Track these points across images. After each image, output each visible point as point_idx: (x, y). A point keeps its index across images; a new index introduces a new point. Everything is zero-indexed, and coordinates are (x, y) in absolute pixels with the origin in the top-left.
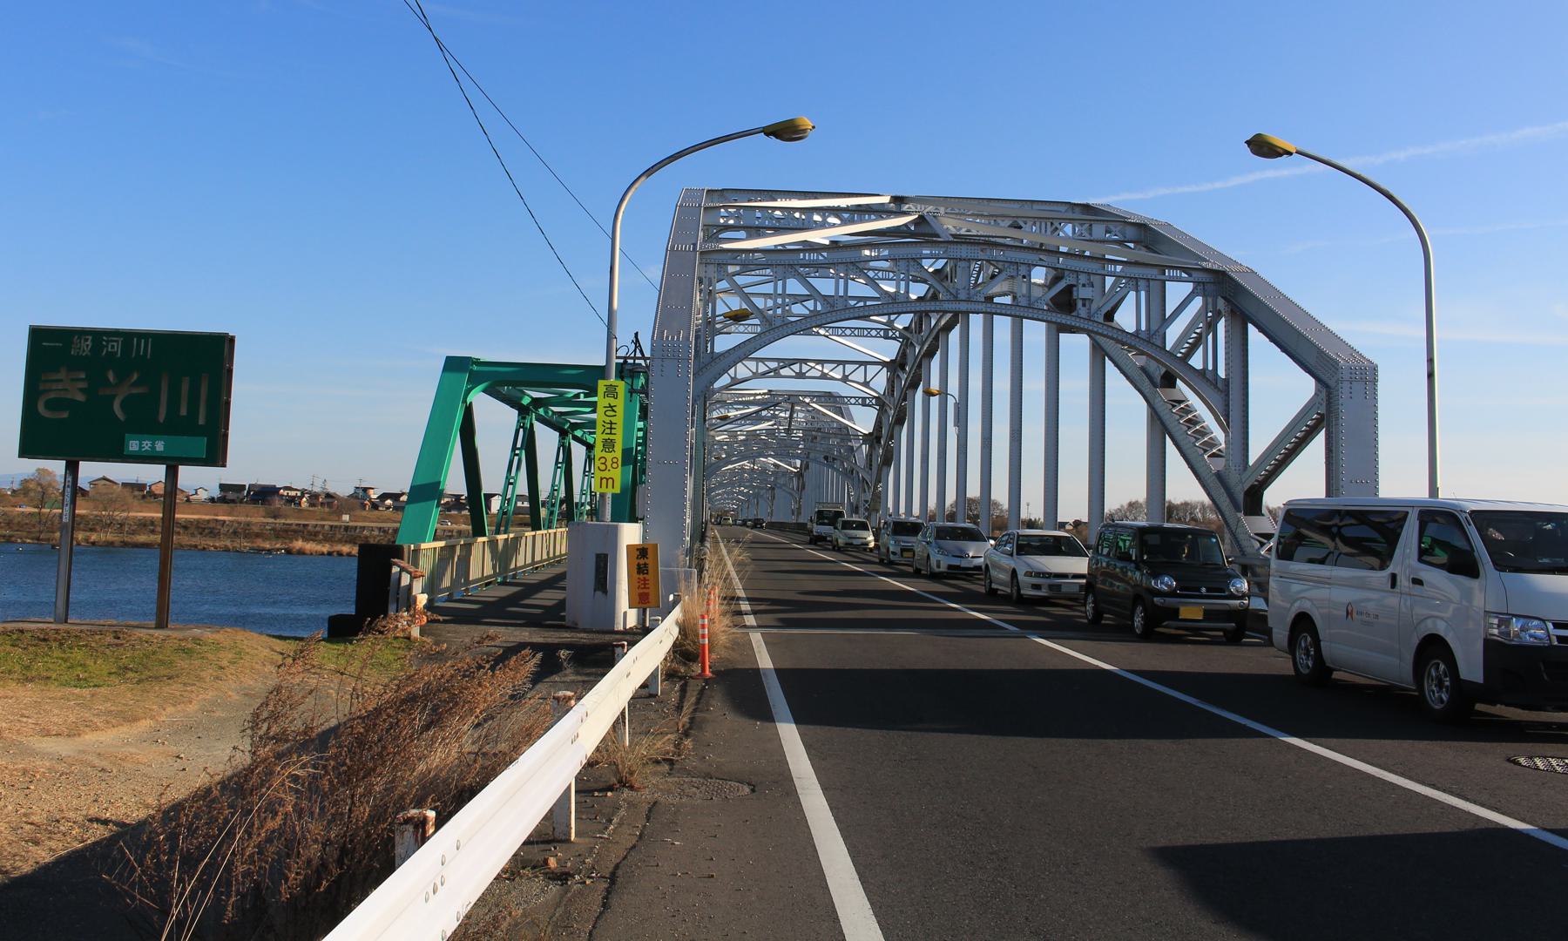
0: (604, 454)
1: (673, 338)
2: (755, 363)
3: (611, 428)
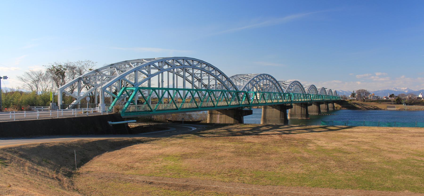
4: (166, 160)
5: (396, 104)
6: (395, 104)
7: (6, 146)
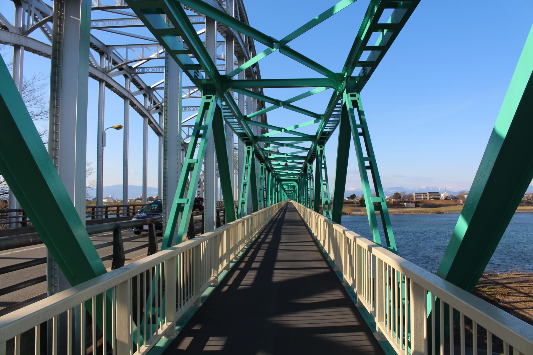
2: (187, 128)
4: (4, 298)
5: (360, 207)
6: (358, 206)
7: (468, 305)
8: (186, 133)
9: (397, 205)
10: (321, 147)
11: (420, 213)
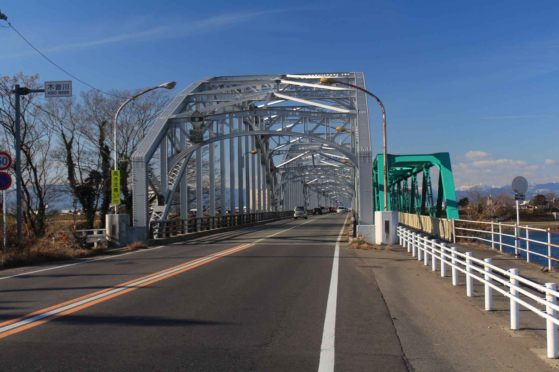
0: (115, 193)
1: (365, 150)
2: (278, 137)
3: (116, 185)
8: (277, 142)
9: (540, 216)
10: (415, 176)
11: (274, 170)
